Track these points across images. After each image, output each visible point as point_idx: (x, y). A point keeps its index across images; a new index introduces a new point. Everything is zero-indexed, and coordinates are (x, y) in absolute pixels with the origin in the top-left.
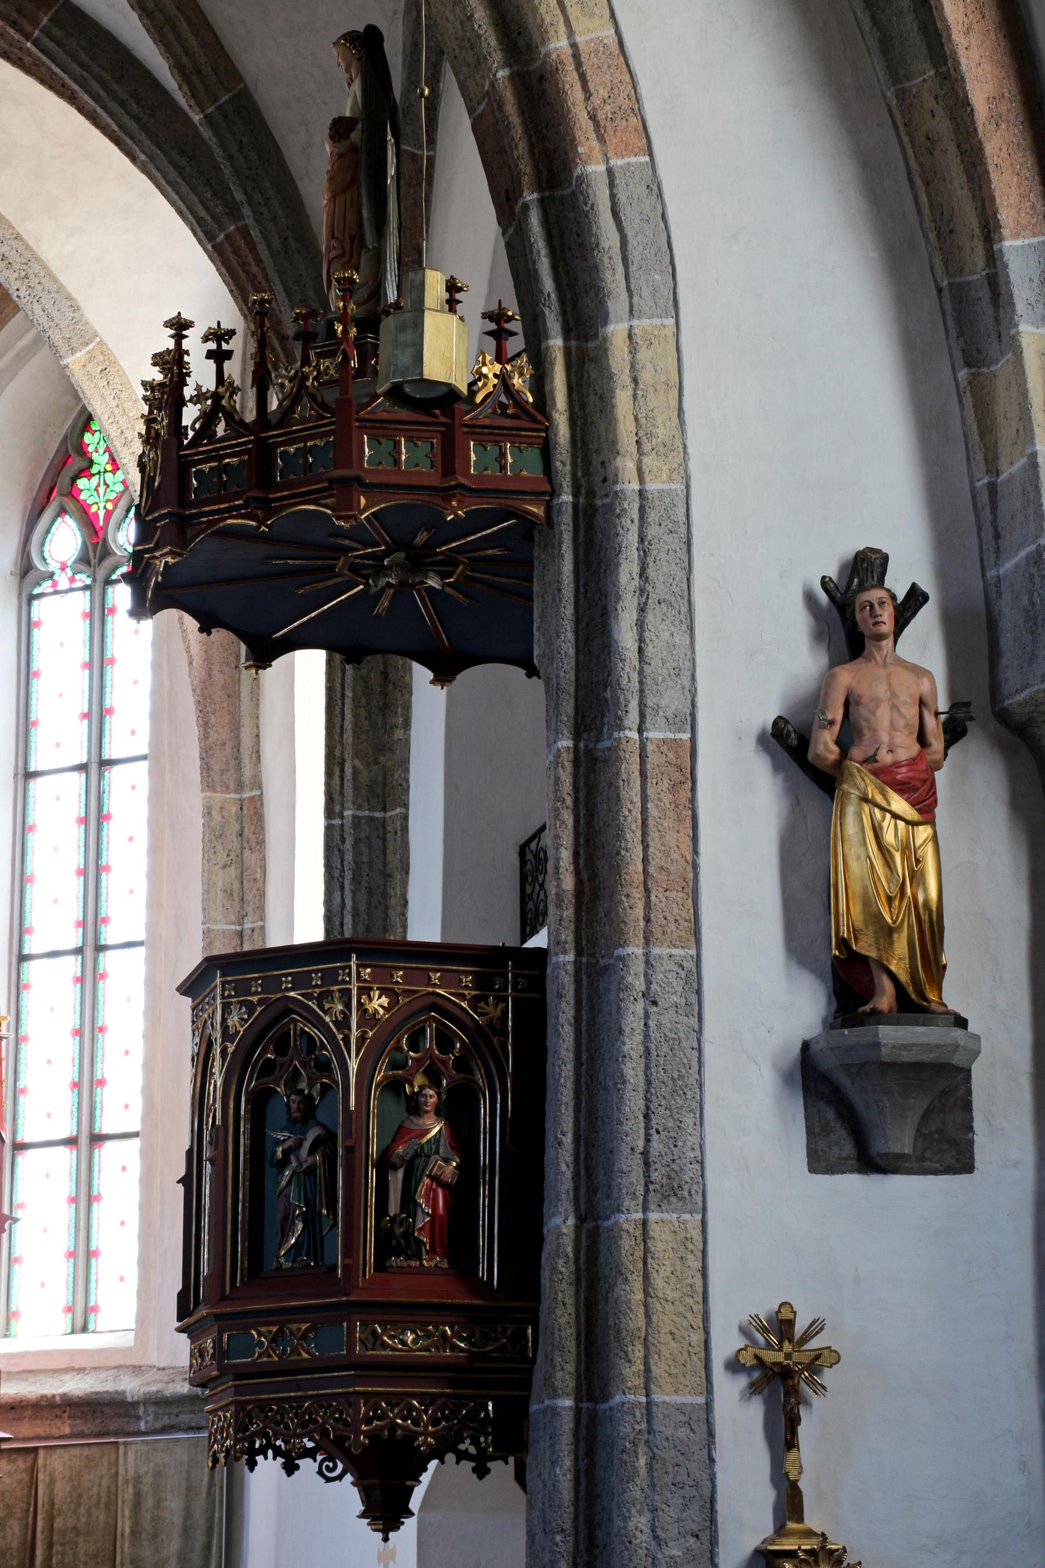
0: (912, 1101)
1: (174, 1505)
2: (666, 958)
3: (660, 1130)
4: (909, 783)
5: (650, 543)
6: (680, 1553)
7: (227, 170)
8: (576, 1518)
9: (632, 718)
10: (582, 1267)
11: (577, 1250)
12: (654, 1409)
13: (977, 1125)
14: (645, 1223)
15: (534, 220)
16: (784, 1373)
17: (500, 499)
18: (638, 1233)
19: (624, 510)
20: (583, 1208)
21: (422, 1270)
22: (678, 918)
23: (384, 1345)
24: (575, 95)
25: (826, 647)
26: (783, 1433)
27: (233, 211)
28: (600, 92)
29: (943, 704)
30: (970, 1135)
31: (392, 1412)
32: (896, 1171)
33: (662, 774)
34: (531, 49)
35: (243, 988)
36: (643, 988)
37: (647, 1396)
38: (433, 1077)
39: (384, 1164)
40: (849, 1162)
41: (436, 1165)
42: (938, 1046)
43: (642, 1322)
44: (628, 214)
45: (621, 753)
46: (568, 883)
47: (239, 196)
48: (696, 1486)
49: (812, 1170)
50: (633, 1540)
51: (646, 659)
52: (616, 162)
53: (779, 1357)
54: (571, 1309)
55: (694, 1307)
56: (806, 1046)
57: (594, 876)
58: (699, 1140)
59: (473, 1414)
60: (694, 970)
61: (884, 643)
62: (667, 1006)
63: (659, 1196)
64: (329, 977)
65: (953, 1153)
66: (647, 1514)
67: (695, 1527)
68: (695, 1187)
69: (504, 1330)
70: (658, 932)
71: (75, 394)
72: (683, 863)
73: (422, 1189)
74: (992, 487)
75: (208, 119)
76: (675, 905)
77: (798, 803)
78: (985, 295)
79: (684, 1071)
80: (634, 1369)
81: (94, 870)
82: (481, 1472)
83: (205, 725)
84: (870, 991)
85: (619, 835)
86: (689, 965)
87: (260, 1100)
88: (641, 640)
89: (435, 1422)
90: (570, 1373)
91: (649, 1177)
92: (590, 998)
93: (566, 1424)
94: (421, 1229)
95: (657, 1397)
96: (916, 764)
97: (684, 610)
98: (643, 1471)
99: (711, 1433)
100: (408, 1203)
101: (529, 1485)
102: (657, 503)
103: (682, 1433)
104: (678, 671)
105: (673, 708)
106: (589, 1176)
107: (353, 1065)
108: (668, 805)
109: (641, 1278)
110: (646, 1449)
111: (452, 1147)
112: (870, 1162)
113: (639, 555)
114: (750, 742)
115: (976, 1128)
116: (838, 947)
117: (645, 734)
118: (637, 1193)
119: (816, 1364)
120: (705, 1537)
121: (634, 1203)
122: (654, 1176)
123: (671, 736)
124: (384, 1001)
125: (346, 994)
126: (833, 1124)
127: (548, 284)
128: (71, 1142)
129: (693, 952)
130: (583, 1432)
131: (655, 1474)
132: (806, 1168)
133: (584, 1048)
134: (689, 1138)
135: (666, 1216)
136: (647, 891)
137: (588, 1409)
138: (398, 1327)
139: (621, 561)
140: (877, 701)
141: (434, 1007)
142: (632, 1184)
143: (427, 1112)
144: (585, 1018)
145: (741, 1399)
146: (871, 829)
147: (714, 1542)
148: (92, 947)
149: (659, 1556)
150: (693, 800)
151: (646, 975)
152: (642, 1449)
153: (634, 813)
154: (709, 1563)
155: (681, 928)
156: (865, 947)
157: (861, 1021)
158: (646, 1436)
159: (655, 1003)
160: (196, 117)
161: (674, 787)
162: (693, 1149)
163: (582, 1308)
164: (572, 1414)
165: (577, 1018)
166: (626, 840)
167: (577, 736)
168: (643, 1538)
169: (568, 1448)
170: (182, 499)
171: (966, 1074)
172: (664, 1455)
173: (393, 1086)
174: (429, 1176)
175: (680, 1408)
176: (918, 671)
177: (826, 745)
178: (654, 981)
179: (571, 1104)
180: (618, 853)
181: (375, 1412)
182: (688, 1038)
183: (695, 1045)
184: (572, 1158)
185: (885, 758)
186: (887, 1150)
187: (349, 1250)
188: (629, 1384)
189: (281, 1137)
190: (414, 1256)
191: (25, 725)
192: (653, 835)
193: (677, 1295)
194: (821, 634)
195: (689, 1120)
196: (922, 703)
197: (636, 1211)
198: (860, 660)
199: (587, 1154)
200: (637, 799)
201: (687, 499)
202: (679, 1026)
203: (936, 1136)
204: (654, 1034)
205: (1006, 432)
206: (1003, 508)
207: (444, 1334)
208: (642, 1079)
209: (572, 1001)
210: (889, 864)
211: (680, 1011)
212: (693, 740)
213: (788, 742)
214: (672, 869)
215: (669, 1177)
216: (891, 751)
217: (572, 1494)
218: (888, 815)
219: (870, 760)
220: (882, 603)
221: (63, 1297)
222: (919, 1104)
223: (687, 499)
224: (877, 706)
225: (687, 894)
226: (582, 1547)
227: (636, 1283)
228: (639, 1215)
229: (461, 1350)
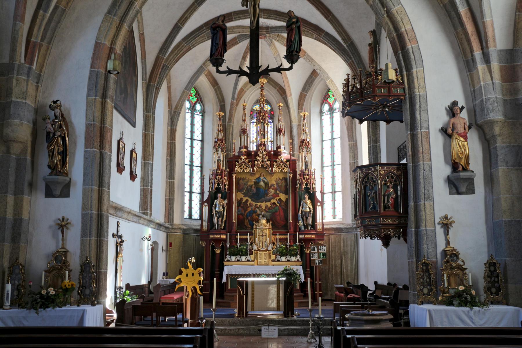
1: (349, 243)
7: (350, 53)
9: (419, 128)
15: (401, 55)
16: (446, 225)
17: (397, 96)
24: (406, 36)
26: (447, 233)
27: (351, 58)
28: (410, 36)
29: (468, 124)
34: (399, 30)
35: (362, 171)
38: (391, 183)
39: (384, 196)
41: (392, 195)
44: (415, 53)
46: (410, 153)
47: (352, 56)
52: (413, 46)
56: (448, 176)
57: (414, 152)
59: (399, 231)
64: (375, 169)
71: (327, 86)
74: (474, 90)
75: (347, 46)
78: (471, 61)
81: (333, 154)
82: (399, 239)
83: (348, 132)
84: (458, 168)
85: (418, 146)
87: (365, 187)
93: (414, 232)
99: (435, 233)
101: (408, 241)
107: (379, 181)
112: (459, 193)
114: (438, 131)
125: (377, 171)
127: (403, 64)
128: (331, 193)
138: (387, 219)
146: (458, 143)
147: (436, 249)
148: (333, 165)
156: (457, 161)
157: (457, 172)
160: (345, 46)
161: (426, 138)
167: (411, 131)
168: (426, 248)
170: (350, 100)
171: (473, 179)
173: (385, 184)
175: (431, 230)
176: (464, 119)
185: (459, 132)
187: (380, 209)
189: (369, 192)
191: (322, 134)
194: (448, 114)
195: (431, 188)
205: (476, 82)
206: (476, 93)
210: (461, 148)
221: (331, 214)
222: (466, 184)
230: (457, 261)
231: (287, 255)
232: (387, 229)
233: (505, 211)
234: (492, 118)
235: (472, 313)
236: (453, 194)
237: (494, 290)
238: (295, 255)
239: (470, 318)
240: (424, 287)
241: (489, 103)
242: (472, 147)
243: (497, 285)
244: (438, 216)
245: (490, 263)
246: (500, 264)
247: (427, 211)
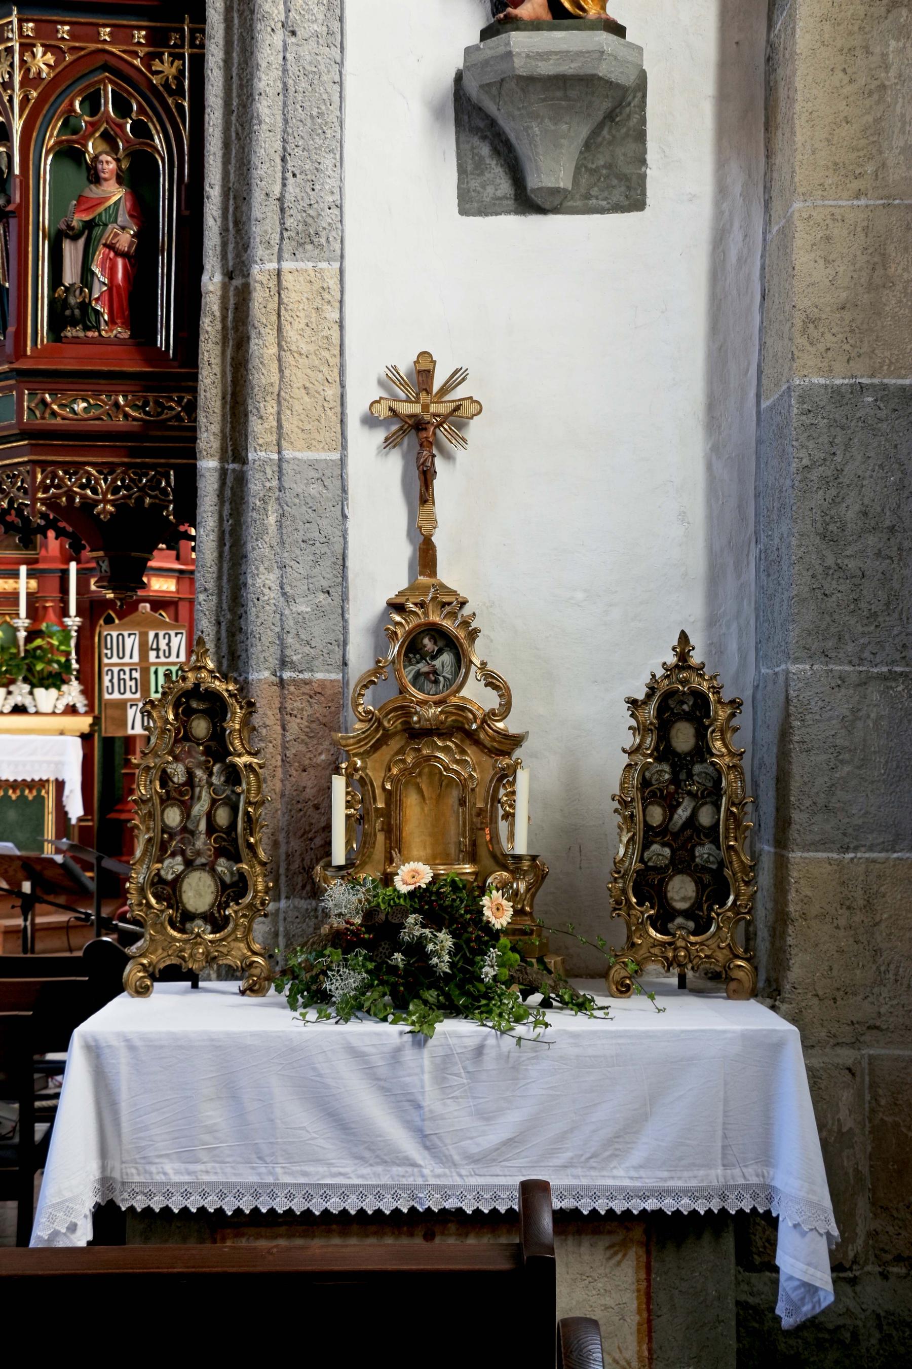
0: (565, 127)
3: (297, 173)
6: (309, 609)
8: (219, 578)
10: (230, 324)
11: (224, 308)
12: (285, 465)
13: (650, 157)
14: (279, 273)
16: (423, 425)
18: (273, 284)
20: (231, 264)
21: (101, 341)
23: (54, 414)
26: (422, 485)
30: (643, 169)
31: (70, 479)
32: (556, 210)
36: (283, 18)
37: (279, 453)
40: (505, 202)
42: (579, 54)
43: (275, 378)
48: (327, 542)
49: (463, 212)
50: (261, 597)
53: (416, 409)
54: (217, 369)
55: (330, 360)
56: (459, 78)
62: (307, 36)
63: (294, 243)
65: (623, 189)
66: (277, 571)
67: (325, 584)
69: (181, 399)
73: (99, 256)
79: (323, 107)
80: (266, 425)
89: (116, 490)
90: (214, 434)
92: (242, 39)
94: (97, 299)
95: (288, 454)
98: (273, 529)
99: (344, 490)
100: (87, 275)
103: (314, 489)
106: (238, 231)
109: (275, 332)
110: (276, 507)
111: (131, 216)
112: (527, 202)
115: (648, 162)
118: (272, 242)
119: (458, 417)
120: (336, 593)
121: (268, 252)
122: (289, 222)
124: (50, 58)
130: (228, 493)
131: (284, 531)
133: (235, 94)
134: (328, 180)
135: (301, 265)
137: (234, 470)
141: (105, 67)
142: (266, 232)
143: (106, 180)
144: (236, 61)
145: (379, 453)
147: (345, 598)
149: (287, 612)
152: (272, 507)
154: (340, 618)
158: (277, 493)
159: (293, 33)
162: (332, 193)
163: (228, 368)
164: (216, 475)
165: (227, 61)
168: (272, 595)
169: (211, 508)
172: (293, 512)
174: (105, 245)
175: (312, 465)
179: (219, 154)
181: (52, 481)
183: (337, 79)
184: (220, 212)
186: (540, 185)
188: (261, 441)
190: (94, 327)
193: (312, 348)
195: (328, 161)
197: (271, 261)
199: (236, 208)
203: (604, 172)
204: (293, 69)
207: (116, 404)
208: (279, 118)
209: (221, 42)
211: (321, 41)
217: (215, 554)
226: (225, 606)
227: (270, 336)
228: (275, 265)
229: (135, 419)
230: (457, 681)
231: (13, 682)
232: (73, 468)
233: (811, 321)
235: (420, 1066)
236: (484, 211)
237: (681, 891)
238: (55, 681)
239: (406, 1104)
240: (189, 864)
243: (692, 859)
244: (371, 364)
245: (669, 694)
246: (735, 704)
247: (291, 333)
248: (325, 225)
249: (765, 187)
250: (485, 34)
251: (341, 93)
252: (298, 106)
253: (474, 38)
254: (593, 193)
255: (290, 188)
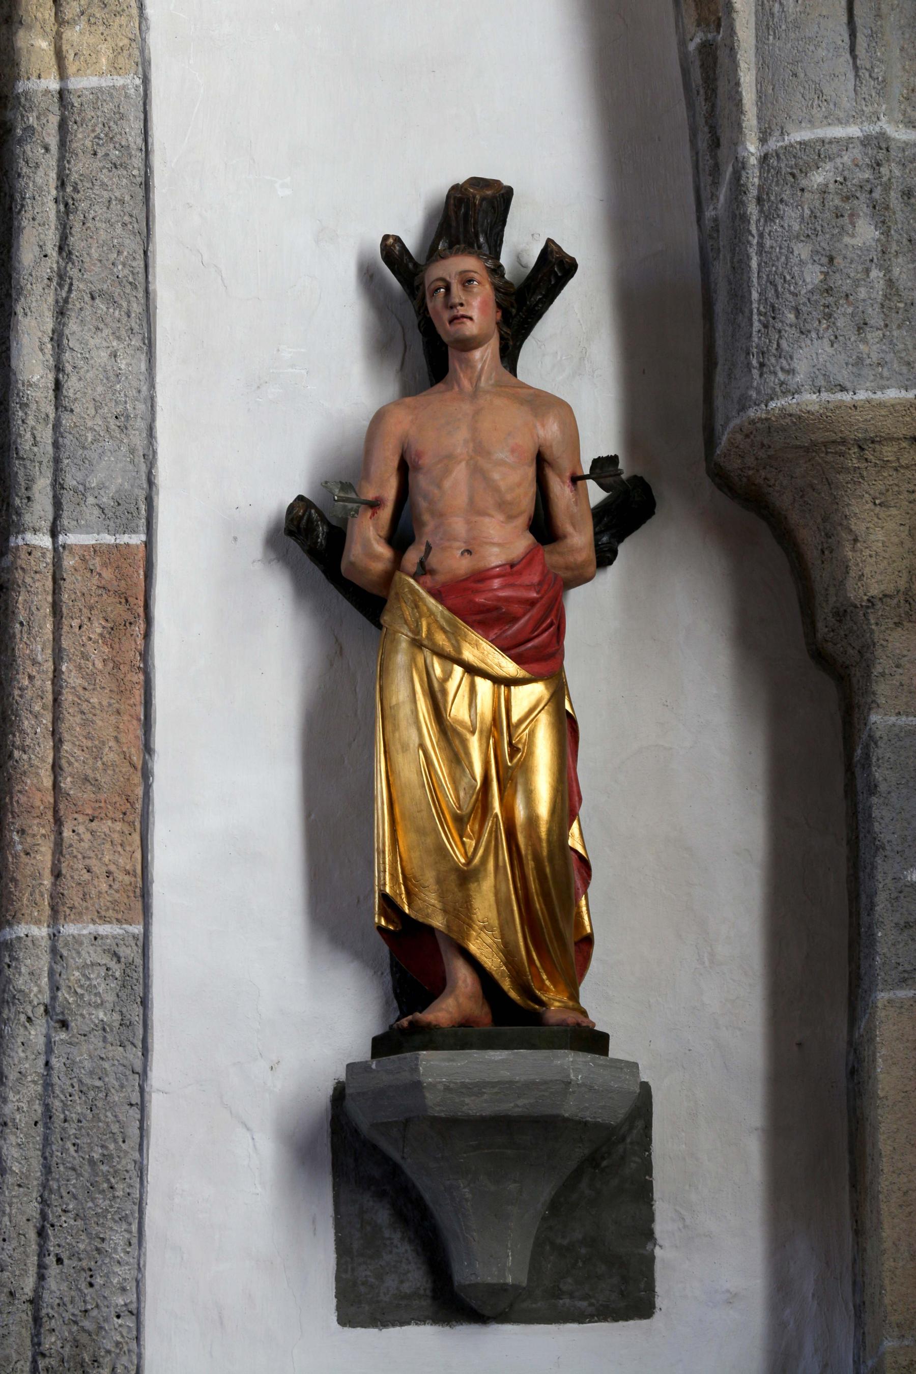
0: (512, 1187)
2: (86, 942)
3: (64, 1256)
4: (497, 608)
5: (76, 190)
13: (660, 1227)
19: (30, 129)
22: (112, 868)
25: (397, 366)
30: (649, 1247)
32: (503, 1317)
33: (91, 608)
36: (46, 998)
42: (530, 1086)
45: (19, 574)
49: (347, 1318)
51: (65, 403)
56: (339, 1094)
58: (135, 1272)
60: (139, 961)
61: (477, 354)
68: (124, 1360)
70: (73, 896)
72: (126, 768)
76: (108, 845)
77: (341, 651)
79: (112, 1146)
86: (130, 952)
88: (59, 368)
91: (39, 1344)
96: (520, 573)
97: (137, 308)
102: (90, 113)
104: (123, 420)
105: (113, 488)
108: (99, 665)
112: (454, 1303)
113: (58, 211)
114: (253, 544)
116: (383, 913)
117: (61, 539)
122: (49, 1342)
123: (109, 539)
126: (387, 1233)
129: (137, 929)
132: (644, 1322)
134: (117, 1269)
136: (58, 821)
139: (25, 223)
140: (449, 459)
150: (146, 654)
151: (51, 973)
153: (38, 683)
155: (116, 886)
159: (64, 1024)
162: (124, 1290)
166: (22, 731)
177: (367, 545)
178: (62, 983)
180: (11, 756)
182: (122, 1086)
183: (135, 1098)
186: (473, 1280)
192: (72, 719)
194: (383, 345)
195: (117, 1237)
196: (541, 461)
198: (440, 386)
200: (45, 656)
201: (145, 104)
202: (106, 1065)
203: (583, 1251)
204: (60, 1081)
210: (457, 757)
211: (110, 1038)
212: (149, 545)
213: (310, 538)
214: (104, 780)
215: (77, 1344)
216: (469, 552)
218: (458, 671)
219: (423, 570)
220: (467, 282)
223: (145, 104)
224: (447, 472)
225: (131, 824)
234: (810, 400)
236: (380, 1318)
241: (791, 217)
242: (645, 738)
248: (110, 1346)
249: (854, 1283)
250: (383, 1045)
251: (142, 1121)
252: (69, 1145)
253: (362, 1051)
254: (565, 1288)
255: (52, 1283)
